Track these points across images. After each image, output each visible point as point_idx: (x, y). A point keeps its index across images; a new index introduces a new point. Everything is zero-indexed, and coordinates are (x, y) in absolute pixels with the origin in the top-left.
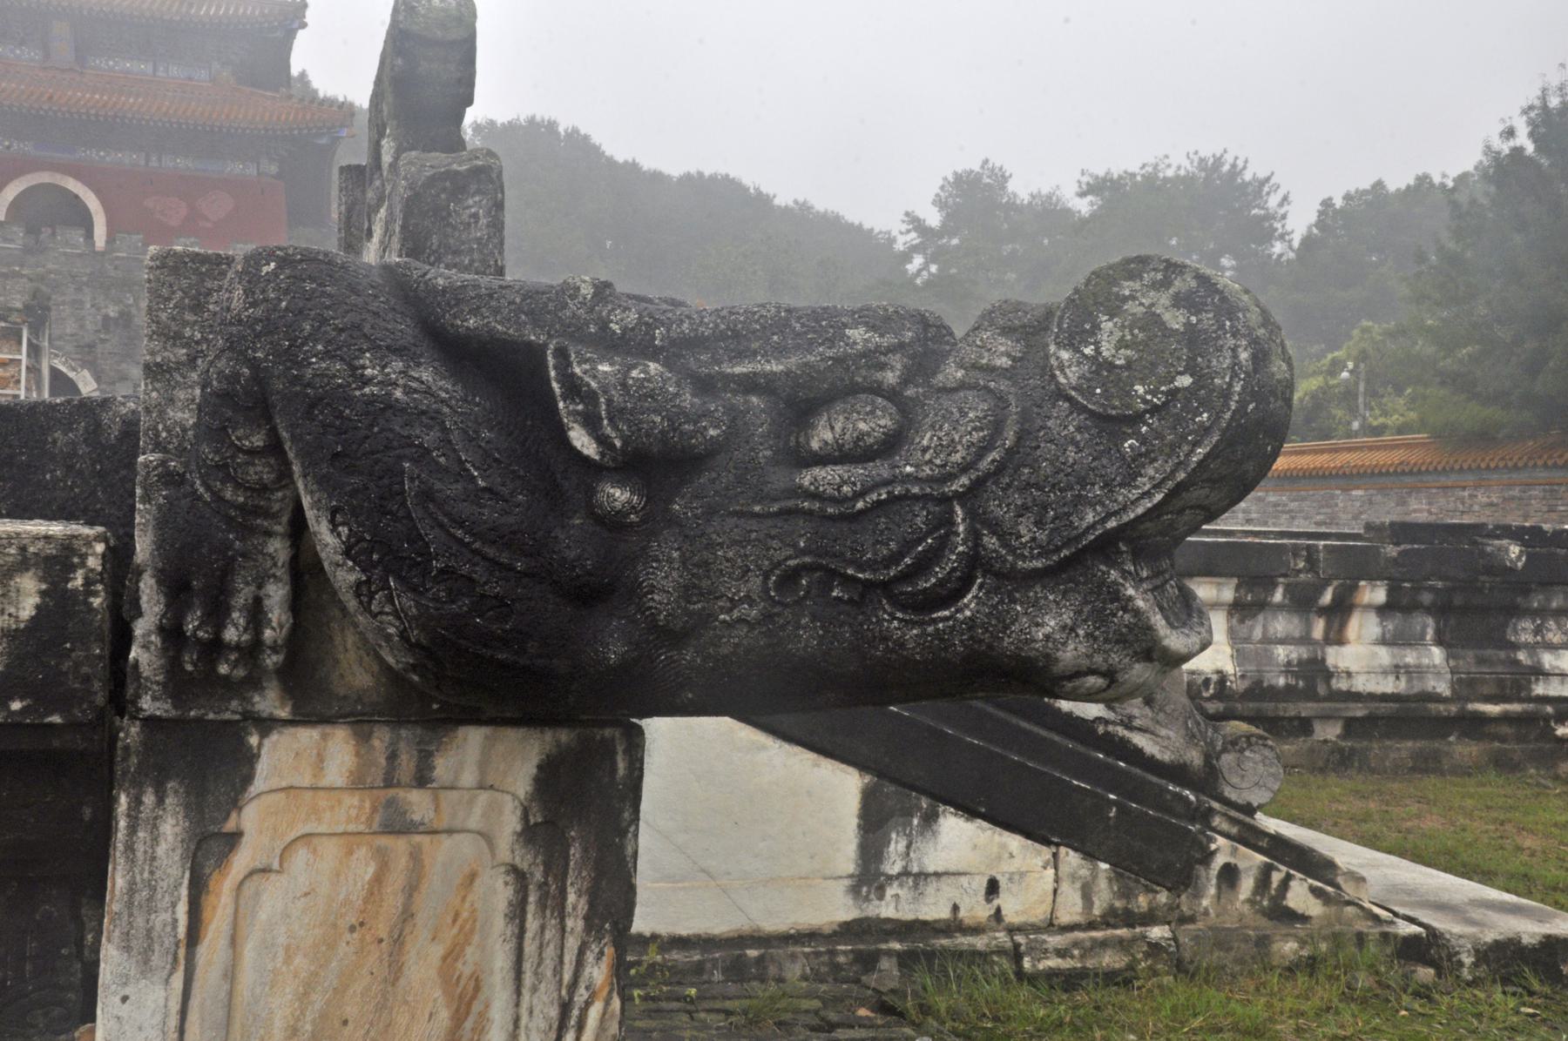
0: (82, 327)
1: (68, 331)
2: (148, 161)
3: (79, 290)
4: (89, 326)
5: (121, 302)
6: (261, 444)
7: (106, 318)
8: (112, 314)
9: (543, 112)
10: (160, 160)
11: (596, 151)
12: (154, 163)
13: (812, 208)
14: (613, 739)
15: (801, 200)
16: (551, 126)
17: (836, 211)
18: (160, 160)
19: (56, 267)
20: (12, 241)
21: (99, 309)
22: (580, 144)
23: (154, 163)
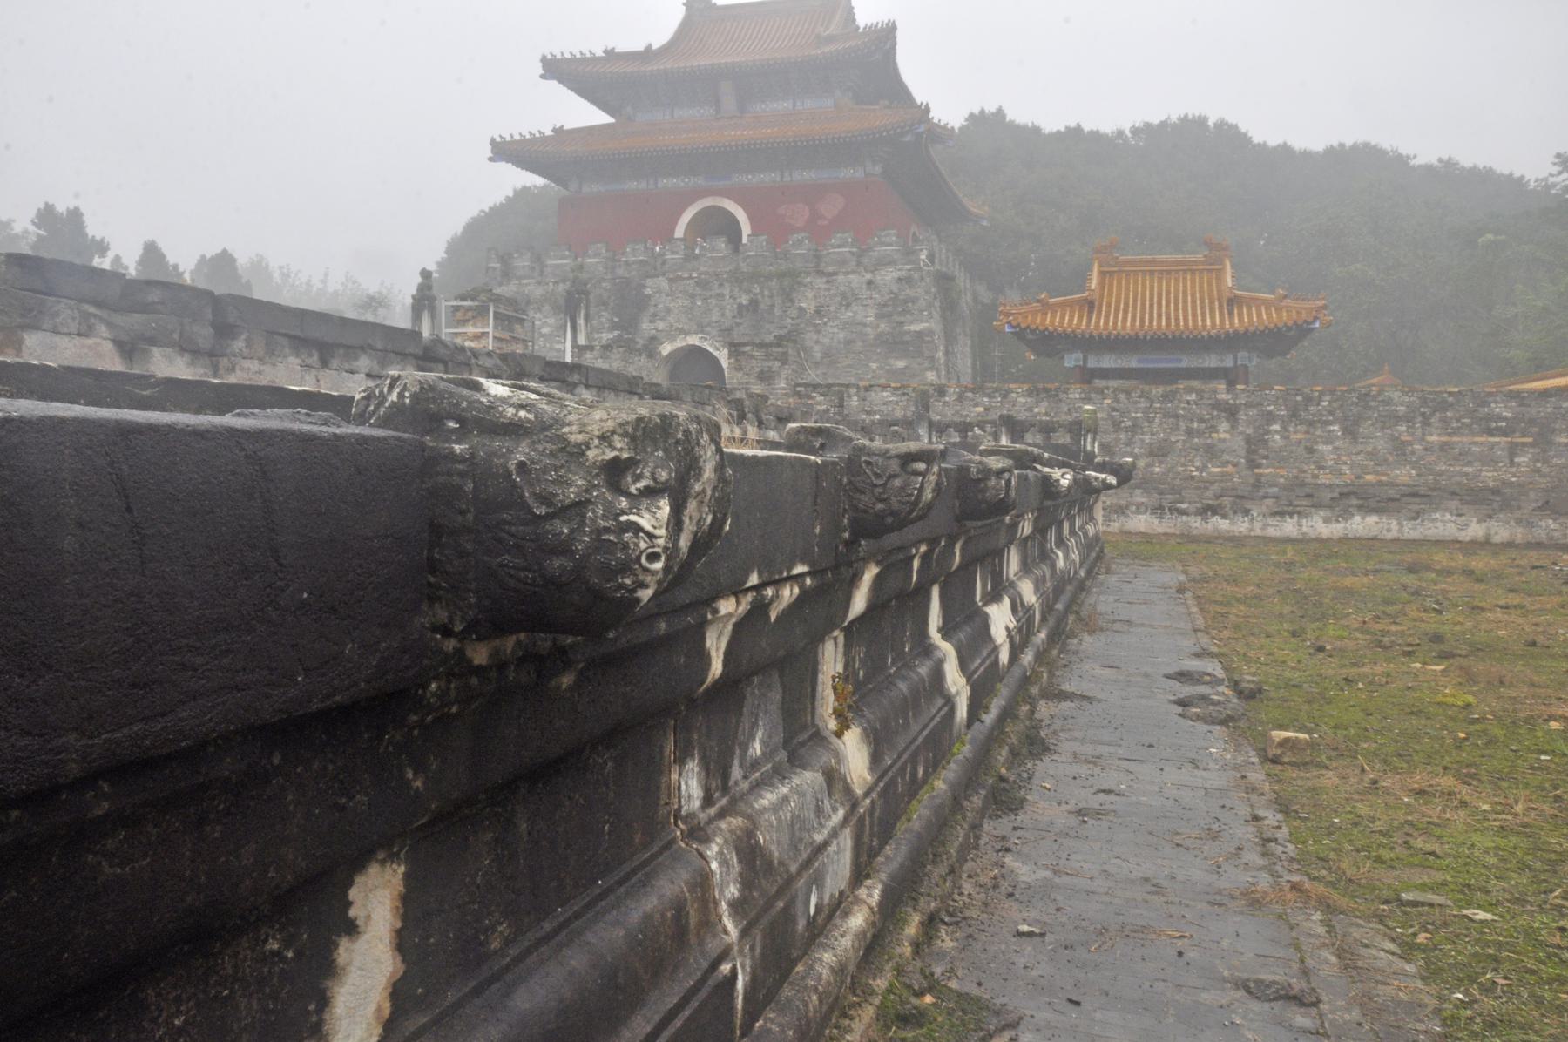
0: (723, 315)
1: (714, 319)
2: (782, 177)
3: (721, 285)
4: (728, 313)
5: (750, 291)
6: (1097, 381)
7: (740, 306)
8: (744, 302)
9: (1194, 110)
10: (791, 175)
11: (1244, 139)
12: (787, 178)
13: (1457, 164)
14: (1003, 765)
15: (1445, 157)
16: (1202, 121)
17: (1488, 165)
18: (791, 175)
19: (706, 269)
20: (677, 253)
21: (735, 299)
22: (1229, 135)
23: (787, 178)
